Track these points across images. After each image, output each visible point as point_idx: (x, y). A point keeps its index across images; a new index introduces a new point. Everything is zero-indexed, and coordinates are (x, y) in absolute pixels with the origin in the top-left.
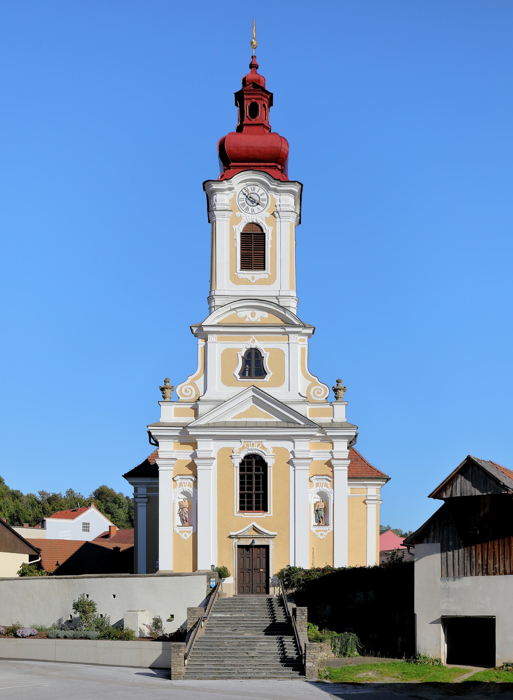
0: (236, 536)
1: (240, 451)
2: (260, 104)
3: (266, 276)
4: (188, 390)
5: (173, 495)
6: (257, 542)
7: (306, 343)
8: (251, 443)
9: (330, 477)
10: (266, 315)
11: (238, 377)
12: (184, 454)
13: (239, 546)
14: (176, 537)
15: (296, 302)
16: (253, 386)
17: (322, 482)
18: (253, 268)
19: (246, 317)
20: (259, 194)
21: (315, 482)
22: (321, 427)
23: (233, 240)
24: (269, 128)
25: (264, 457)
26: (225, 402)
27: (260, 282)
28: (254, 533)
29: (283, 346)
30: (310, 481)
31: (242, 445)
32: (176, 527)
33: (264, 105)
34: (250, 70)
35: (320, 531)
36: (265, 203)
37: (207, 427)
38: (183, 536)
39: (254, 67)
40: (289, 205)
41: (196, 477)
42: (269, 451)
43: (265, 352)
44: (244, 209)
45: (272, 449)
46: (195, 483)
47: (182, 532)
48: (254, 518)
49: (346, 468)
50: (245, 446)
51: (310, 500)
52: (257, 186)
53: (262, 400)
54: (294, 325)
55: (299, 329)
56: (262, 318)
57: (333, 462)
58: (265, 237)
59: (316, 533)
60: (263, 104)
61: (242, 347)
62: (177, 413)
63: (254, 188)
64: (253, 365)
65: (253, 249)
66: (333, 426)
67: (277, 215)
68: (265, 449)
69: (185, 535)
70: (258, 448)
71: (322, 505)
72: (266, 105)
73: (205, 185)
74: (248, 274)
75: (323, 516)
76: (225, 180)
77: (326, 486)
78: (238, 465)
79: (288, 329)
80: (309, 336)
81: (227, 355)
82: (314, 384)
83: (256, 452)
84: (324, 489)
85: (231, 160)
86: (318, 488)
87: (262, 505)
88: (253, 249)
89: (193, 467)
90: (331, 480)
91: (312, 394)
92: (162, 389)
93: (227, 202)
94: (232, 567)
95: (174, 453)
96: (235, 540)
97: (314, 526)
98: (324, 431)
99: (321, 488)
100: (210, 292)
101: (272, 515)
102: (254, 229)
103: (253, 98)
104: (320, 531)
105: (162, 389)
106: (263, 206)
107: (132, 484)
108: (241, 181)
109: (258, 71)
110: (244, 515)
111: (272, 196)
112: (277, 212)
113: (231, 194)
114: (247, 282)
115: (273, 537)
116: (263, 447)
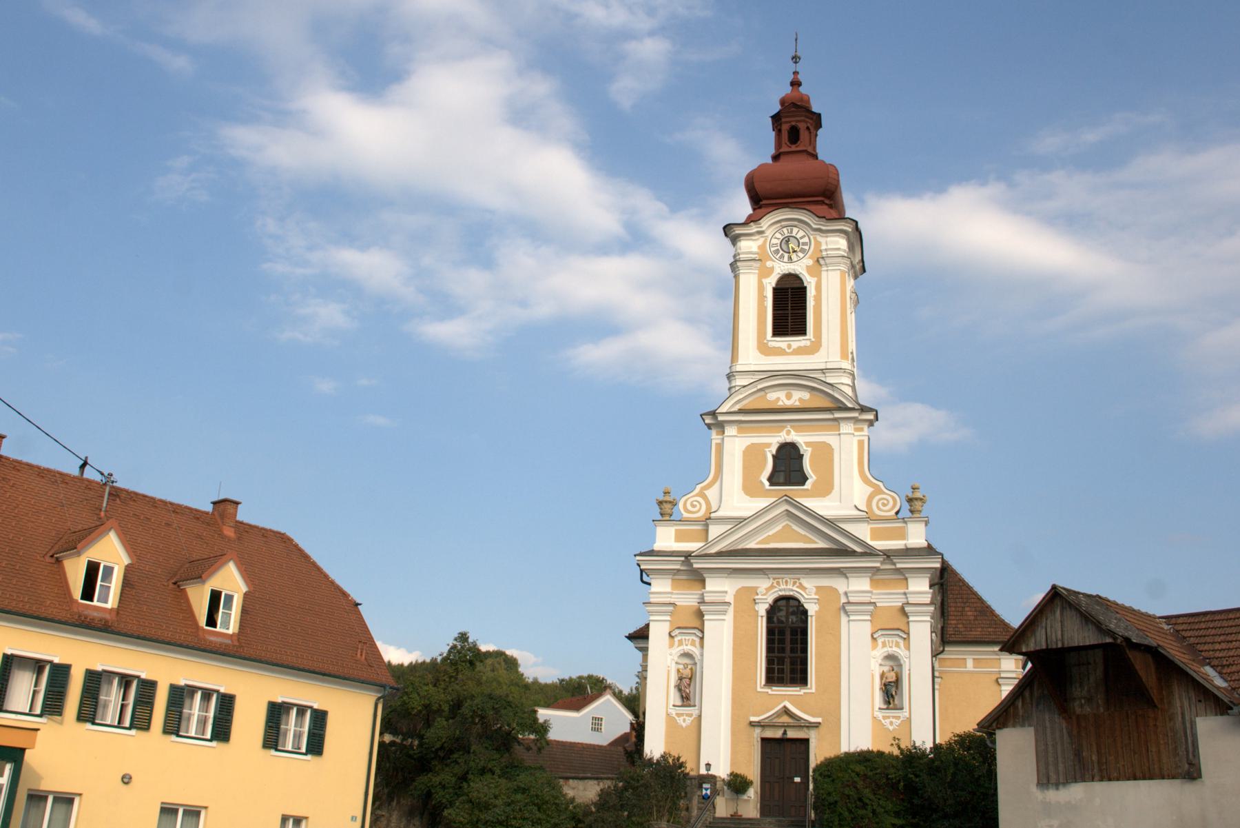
1: (766, 592)
2: (802, 126)
3: (808, 343)
6: (792, 734)
10: (806, 395)
11: (767, 484)
12: (687, 599)
13: (763, 740)
14: (670, 720)
19: (778, 399)
21: (880, 641)
22: (888, 555)
23: (761, 298)
24: (815, 156)
25: (802, 600)
27: (800, 351)
28: (785, 719)
30: (874, 639)
37: (720, 554)
38: (680, 720)
41: (702, 632)
42: (808, 592)
46: (702, 647)
47: (678, 715)
48: (786, 696)
49: (928, 618)
55: (855, 414)
56: (800, 400)
57: (907, 609)
61: (773, 441)
62: (680, 537)
64: (788, 468)
66: (908, 552)
67: (822, 262)
68: (804, 589)
74: (782, 342)
77: (897, 645)
79: (837, 415)
81: (751, 454)
82: (877, 491)
84: (894, 650)
85: (763, 197)
87: (798, 676)
89: (700, 615)
91: (875, 508)
92: (660, 503)
93: (755, 249)
94: (753, 771)
96: (758, 730)
101: (813, 690)
103: (795, 123)
105: (660, 503)
106: (803, 251)
108: (772, 225)
109: (801, 89)
114: (780, 352)
115: (816, 726)
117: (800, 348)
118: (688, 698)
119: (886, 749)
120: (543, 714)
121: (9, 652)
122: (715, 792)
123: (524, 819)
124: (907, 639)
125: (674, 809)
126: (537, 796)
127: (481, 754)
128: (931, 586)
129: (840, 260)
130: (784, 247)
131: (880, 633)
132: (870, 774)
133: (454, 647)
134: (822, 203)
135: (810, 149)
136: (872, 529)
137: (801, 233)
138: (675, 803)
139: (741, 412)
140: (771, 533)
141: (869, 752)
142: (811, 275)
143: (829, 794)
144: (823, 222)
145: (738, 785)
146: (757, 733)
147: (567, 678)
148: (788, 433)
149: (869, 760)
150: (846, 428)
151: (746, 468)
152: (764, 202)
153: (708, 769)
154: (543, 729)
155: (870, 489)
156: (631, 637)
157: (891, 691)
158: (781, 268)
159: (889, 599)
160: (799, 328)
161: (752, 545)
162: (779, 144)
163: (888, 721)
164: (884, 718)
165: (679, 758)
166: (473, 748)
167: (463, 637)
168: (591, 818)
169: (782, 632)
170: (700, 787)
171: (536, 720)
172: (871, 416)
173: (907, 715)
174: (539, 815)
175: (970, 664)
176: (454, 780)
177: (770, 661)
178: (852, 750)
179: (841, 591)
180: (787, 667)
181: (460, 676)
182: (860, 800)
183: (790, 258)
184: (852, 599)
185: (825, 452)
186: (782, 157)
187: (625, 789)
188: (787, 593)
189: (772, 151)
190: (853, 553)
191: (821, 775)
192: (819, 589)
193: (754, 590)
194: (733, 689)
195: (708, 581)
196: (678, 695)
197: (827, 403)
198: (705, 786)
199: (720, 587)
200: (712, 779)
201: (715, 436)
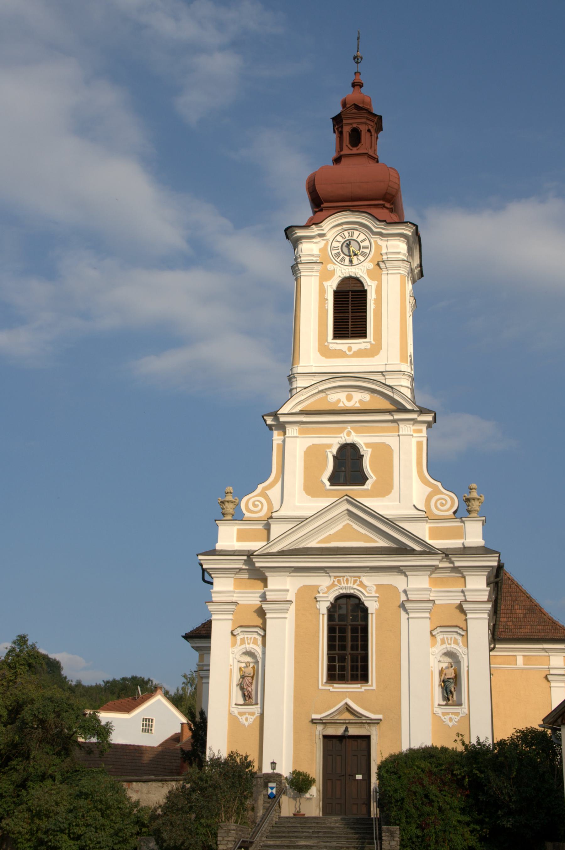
0: (320, 720)
1: (328, 589)
2: (363, 129)
3: (368, 346)
4: (257, 503)
5: (231, 656)
6: (353, 731)
7: (424, 433)
8: (345, 579)
9: (462, 628)
10: (367, 396)
11: (328, 483)
12: (250, 597)
13: (325, 737)
14: (233, 720)
15: (410, 379)
16: (347, 495)
17: (449, 636)
18: (350, 335)
19: (339, 401)
20: (359, 240)
21: (439, 637)
22: (447, 554)
23: (323, 300)
24: (376, 160)
25: (363, 598)
26: (307, 519)
27: (360, 354)
28: (347, 716)
29: (390, 440)
30: (432, 635)
31: (332, 581)
32: (234, 706)
33: (369, 131)
34: (352, 89)
35: (448, 714)
36: (367, 251)
37: (282, 553)
38: (242, 719)
39: (357, 85)
40: (399, 253)
41: (264, 630)
43: (365, 449)
44: (338, 260)
45: (375, 587)
47: (241, 714)
48: (348, 693)
49: (486, 616)
50: (336, 583)
51: (432, 664)
52: (356, 230)
53: (361, 516)
54: (405, 410)
57: (465, 606)
58: (366, 295)
59: (443, 718)
60: (367, 129)
61: (334, 442)
62: (242, 536)
63: (353, 233)
64: (348, 467)
65: (350, 311)
66: (465, 551)
67: (382, 265)
68: (365, 587)
69: (247, 719)
70: (355, 586)
71: (450, 674)
72: (373, 131)
73: (381, 219)
74: (343, 344)
75: (453, 690)
76: (313, 224)
77: (456, 642)
78: (325, 611)
79: (397, 416)
80: (429, 425)
81: (313, 454)
82: (436, 491)
83: (352, 591)
84: (453, 647)
86: (444, 646)
87: (361, 675)
88: (350, 311)
89: (261, 613)
90: (463, 633)
93: (316, 252)
94: (314, 769)
95: (235, 595)
96: (320, 727)
97: (439, 705)
98: (450, 559)
99: (448, 646)
100: (291, 369)
101: (374, 687)
102: (352, 285)
104: (448, 714)
106: (363, 254)
107: (197, 649)
110: (334, 688)
111: (376, 242)
112: (383, 261)
113: (321, 243)
114: (341, 354)
115: (377, 722)
116: (362, 584)
117: (360, 350)
118: (250, 697)
119: (450, 745)
120: (104, 716)
121: (372, 737)
122: (281, 791)
123: (88, 825)
124: (465, 637)
125: (241, 809)
126: (101, 801)
127: (42, 758)
128: (488, 585)
129: (400, 263)
130: (345, 250)
131: (439, 630)
132: (435, 770)
133: (12, 651)
134: (383, 206)
135: (371, 153)
136: (430, 528)
137: (362, 237)
138: (242, 804)
139: (303, 413)
140: (332, 532)
141: (433, 748)
142: (372, 279)
143: (396, 791)
144: (382, 225)
145: (300, 783)
146: (319, 730)
147: (111, 679)
148: (349, 434)
149: (432, 756)
150: (406, 429)
151: (307, 468)
152: (325, 205)
153: (274, 768)
154: (104, 732)
155: (430, 490)
156: (187, 637)
157: (451, 688)
158: (343, 271)
159: (447, 596)
160: (360, 331)
161: (313, 543)
162: (341, 147)
163: (447, 717)
164: (444, 714)
165: (246, 757)
166: (33, 754)
167: (22, 640)
168: (159, 821)
169: (343, 630)
170: (266, 786)
171: (98, 721)
172: (429, 418)
173: (466, 711)
174: (102, 820)
175: (520, 660)
176: (12, 787)
177: (331, 659)
178: (416, 745)
179: (401, 589)
180: (348, 664)
181: (19, 680)
182: (427, 796)
183: (351, 261)
184: (411, 597)
185: (384, 453)
186: (343, 160)
187: (193, 790)
188: (348, 591)
189: (334, 155)
190: (410, 552)
191: (387, 772)
192: (379, 587)
193: (316, 589)
194: (295, 687)
195: (270, 580)
196: (240, 693)
197: (387, 405)
198: (270, 785)
199: (283, 585)
200: (276, 777)
201: (277, 437)
